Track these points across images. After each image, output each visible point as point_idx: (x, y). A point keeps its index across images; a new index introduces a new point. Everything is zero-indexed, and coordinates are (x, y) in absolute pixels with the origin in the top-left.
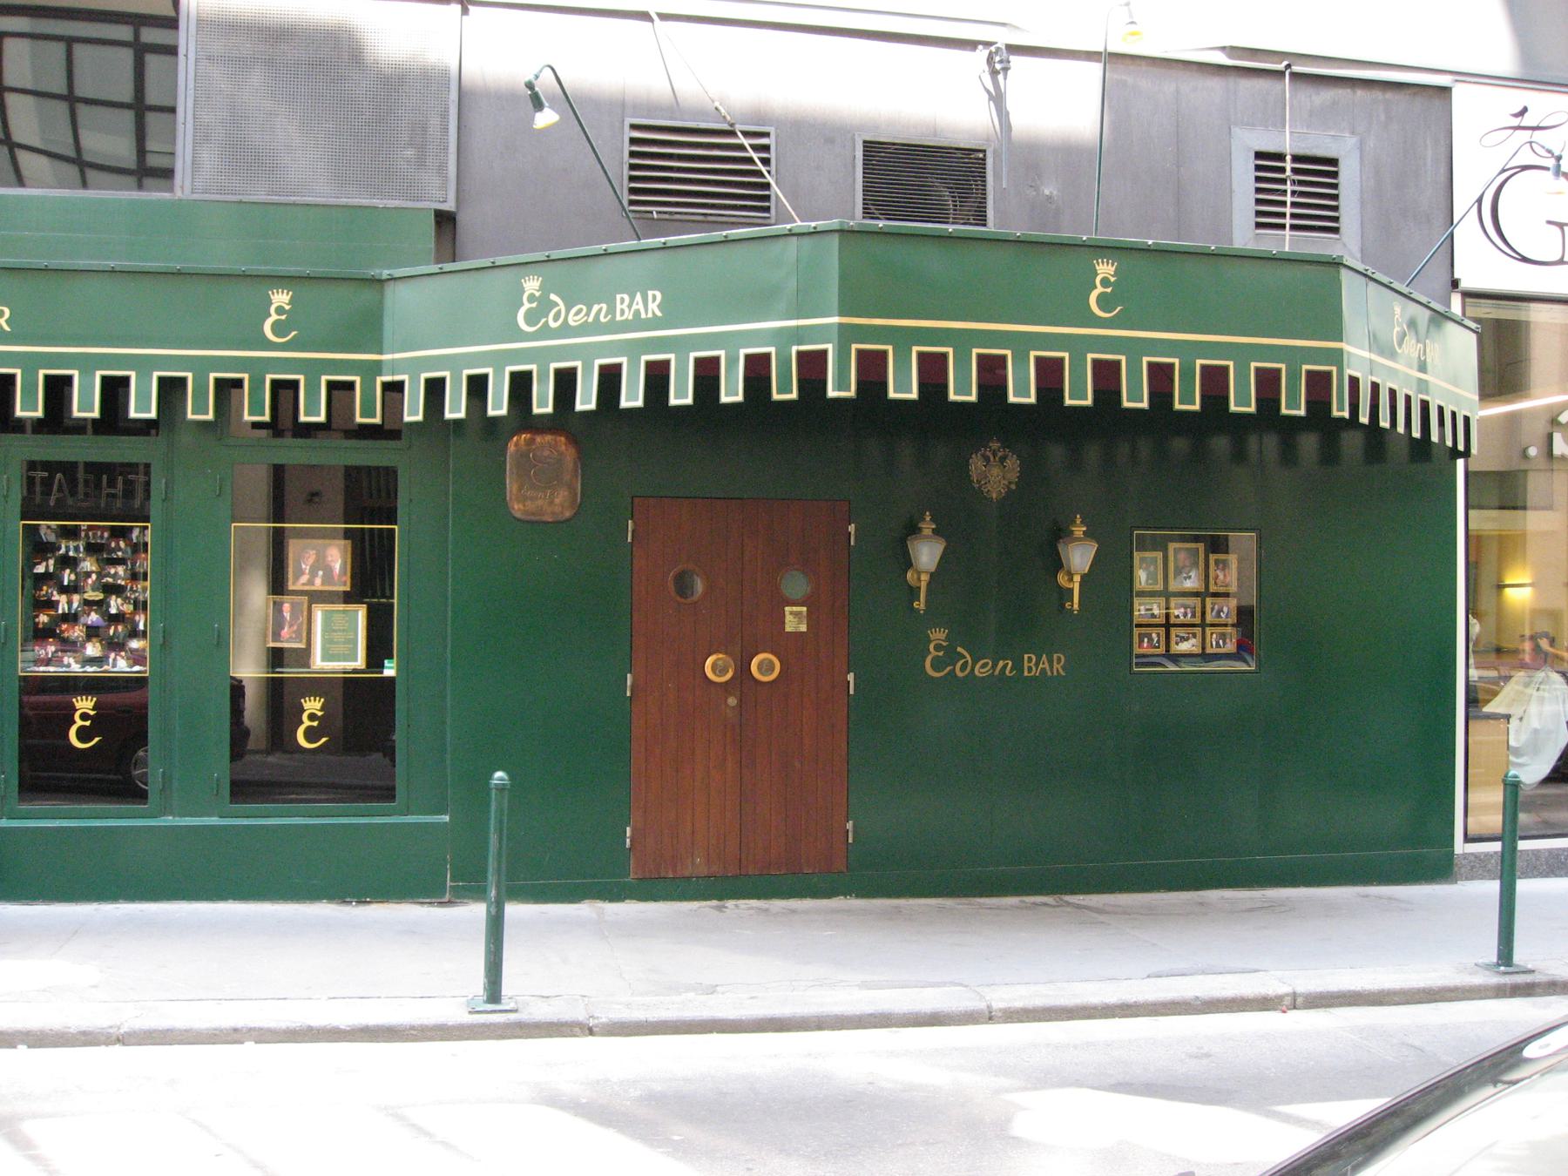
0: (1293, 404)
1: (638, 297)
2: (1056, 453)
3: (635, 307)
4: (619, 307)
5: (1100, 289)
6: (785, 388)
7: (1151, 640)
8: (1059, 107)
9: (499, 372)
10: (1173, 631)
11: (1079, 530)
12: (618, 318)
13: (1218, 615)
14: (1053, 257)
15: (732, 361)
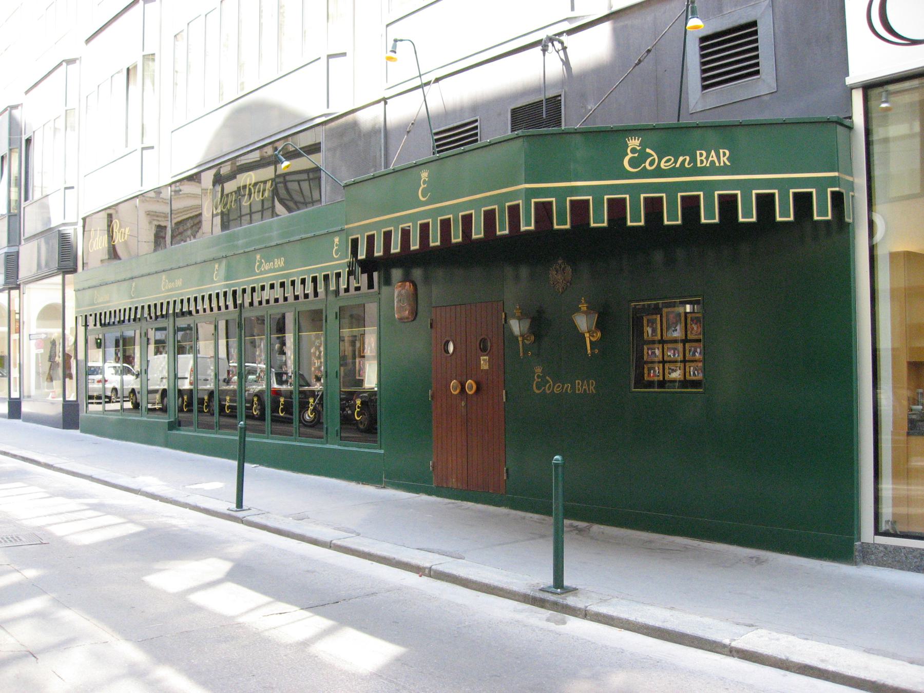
0: (785, 213)
1: (713, 153)
2: (417, 273)
3: (710, 159)
4: (699, 159)
5: (630, 155)
6: (562, 221)
7: (655, 371)
8: (593, 49)
9: (396, 229)
10: (667, 366)
11: (584, 307)
12: (699, 165)
13: (694, 354)
14: (606, 140)
15: (478, 215)
